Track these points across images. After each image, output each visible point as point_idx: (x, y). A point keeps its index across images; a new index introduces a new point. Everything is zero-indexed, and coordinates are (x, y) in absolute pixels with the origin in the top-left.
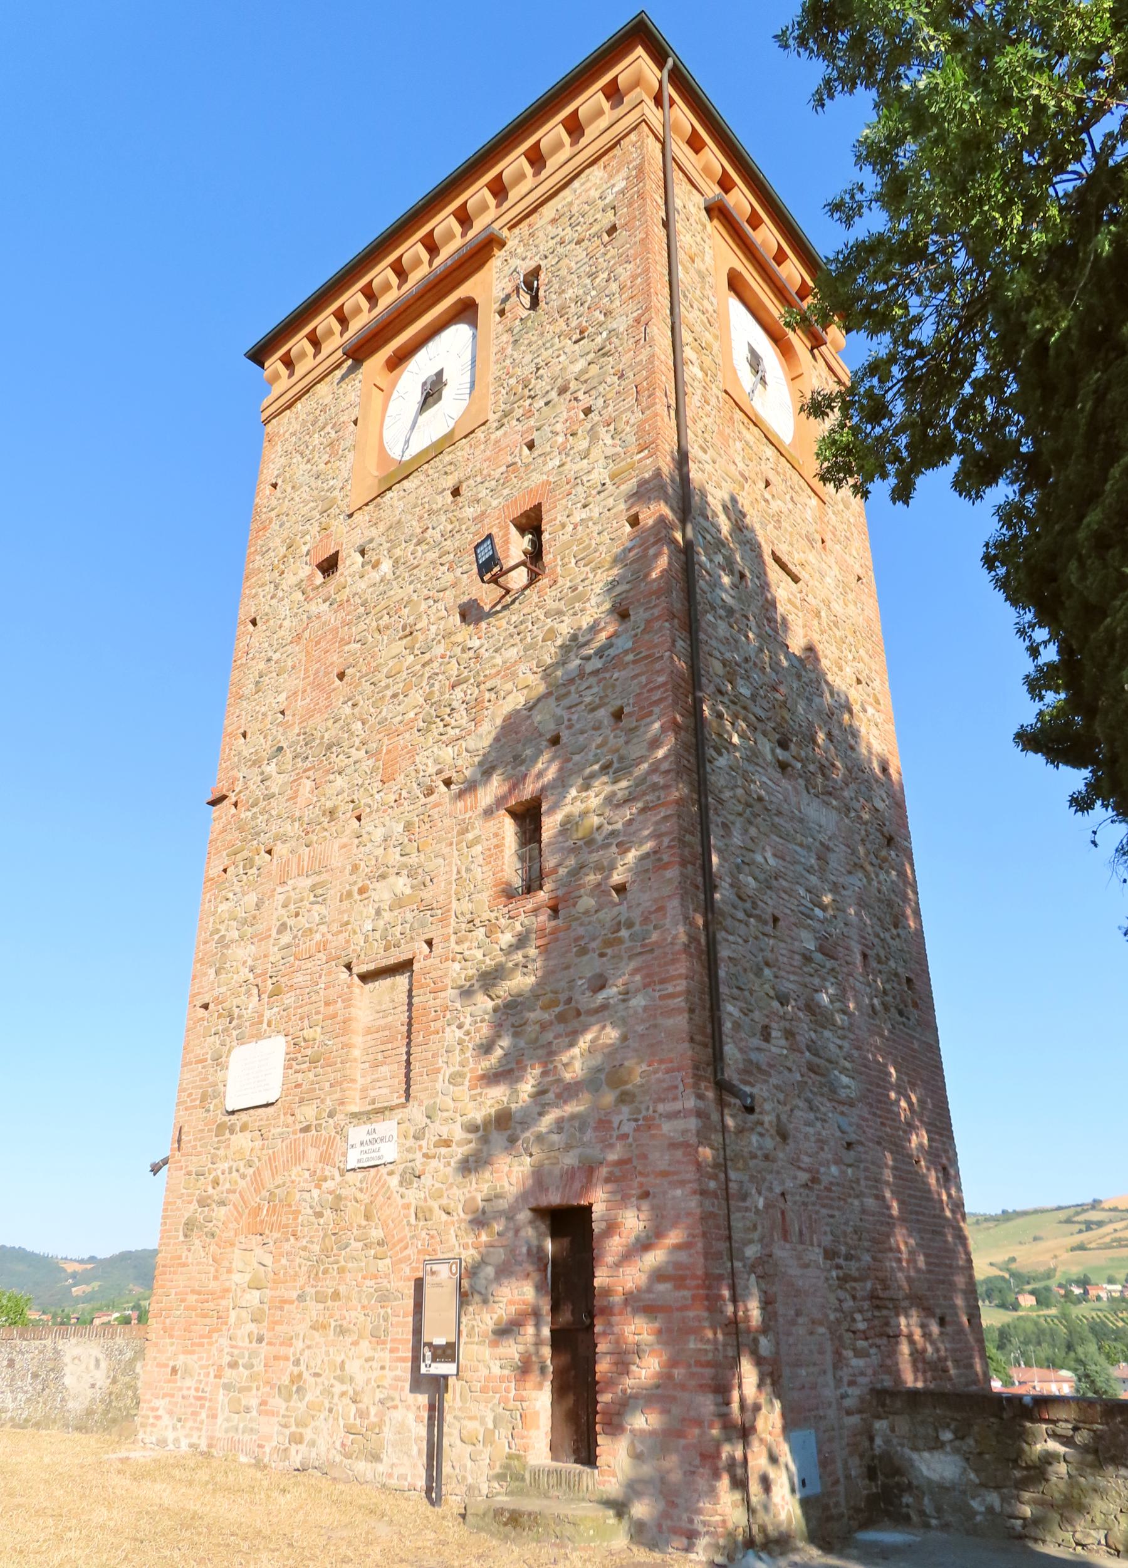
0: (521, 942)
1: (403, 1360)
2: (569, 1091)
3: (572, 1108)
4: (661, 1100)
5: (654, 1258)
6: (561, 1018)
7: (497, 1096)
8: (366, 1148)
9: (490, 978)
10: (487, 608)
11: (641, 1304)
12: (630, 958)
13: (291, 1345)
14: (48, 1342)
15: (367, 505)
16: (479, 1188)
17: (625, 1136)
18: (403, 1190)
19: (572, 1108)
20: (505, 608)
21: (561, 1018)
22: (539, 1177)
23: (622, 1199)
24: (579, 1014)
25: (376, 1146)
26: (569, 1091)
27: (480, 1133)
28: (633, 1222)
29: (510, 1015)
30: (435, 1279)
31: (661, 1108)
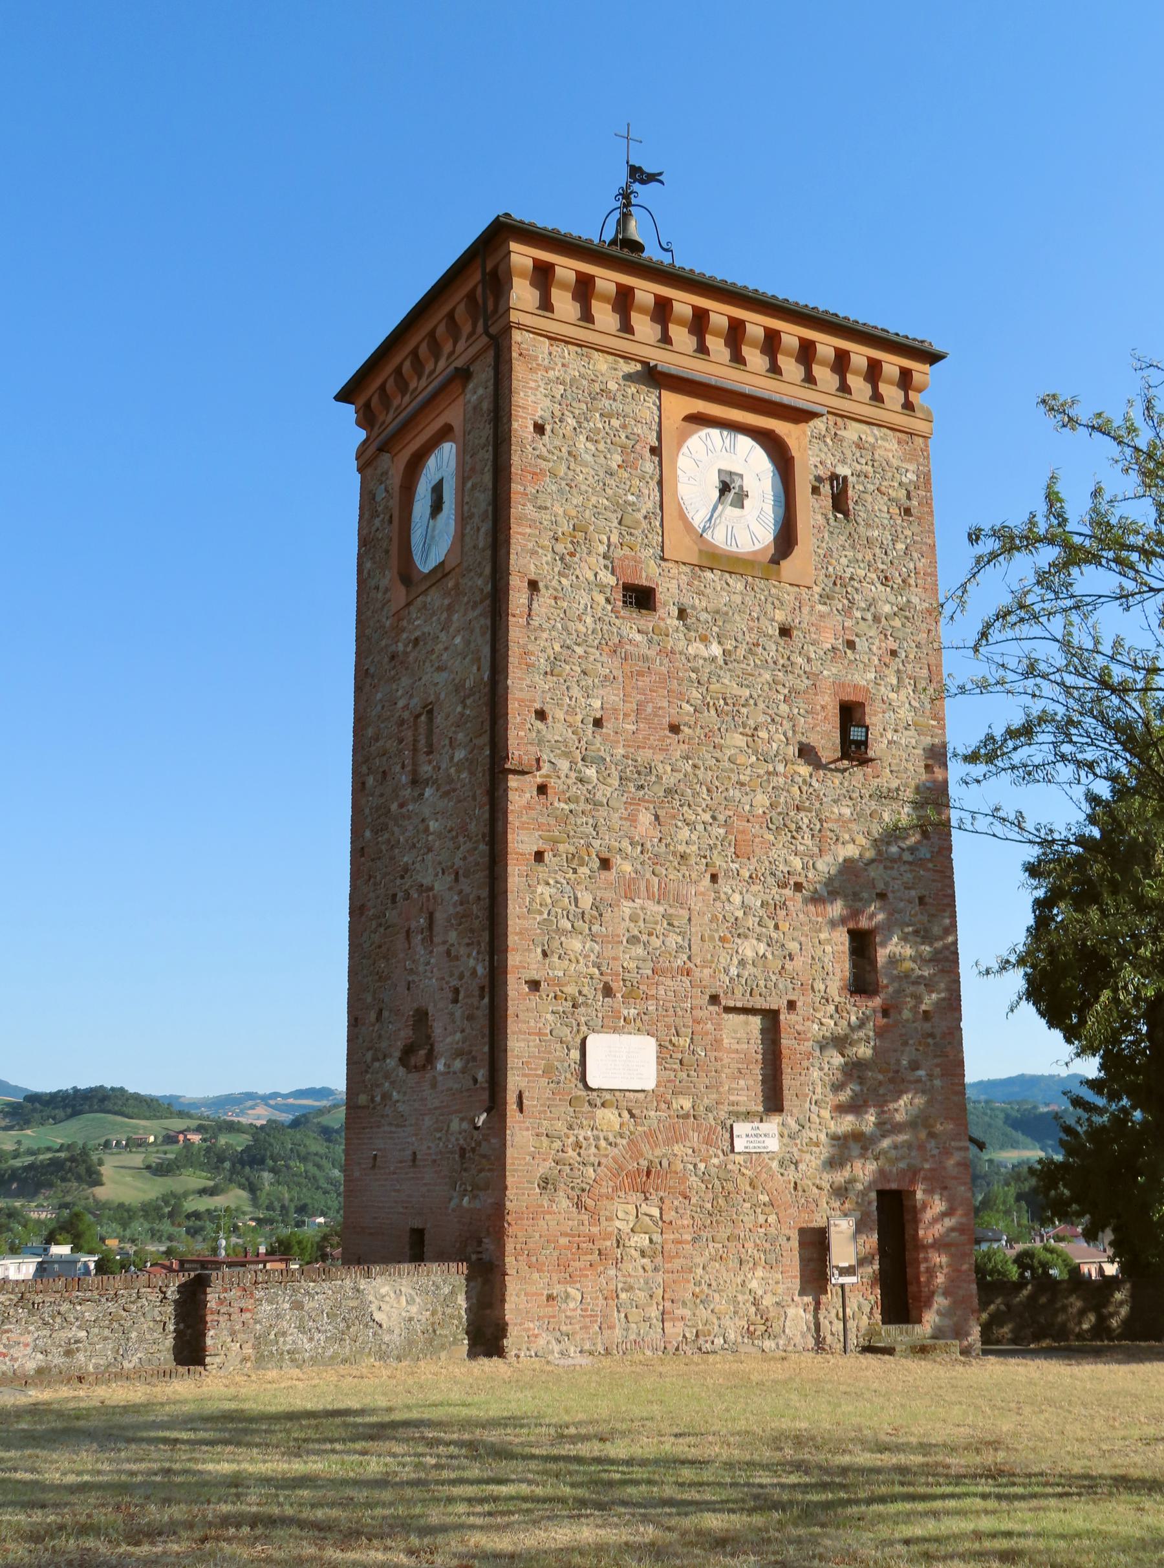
0: (862, 1024)
1: (795, 1277)
2: (898, 1128)
3: (902, 1138)
4: (953, 1140)
5: (948, 1222)
6: (892, 1081)
7: (848, 1123)
8: (751, 1139)
9: (840, 1042)
10: (824, 761)
11: (940, 1245)
12: (935, 1056)
13: (691, 1272)
14: (348, 1283)
15: (684, 564)
16: (840, 1177)
17: (933, 1156)
18: (782, 1171)
19: (902, 1138)
20: (837, 770)
21: (892, 1081)
22: (881, 1172)
23: (929, 1192)
24: (903, 1081)
25: (760, 1139)
26: (898, 1128)
27: (841, 1142)
28: (938, 1205)
29: (854, 1070)
30: (837, 1229)
31: (953, 1144)
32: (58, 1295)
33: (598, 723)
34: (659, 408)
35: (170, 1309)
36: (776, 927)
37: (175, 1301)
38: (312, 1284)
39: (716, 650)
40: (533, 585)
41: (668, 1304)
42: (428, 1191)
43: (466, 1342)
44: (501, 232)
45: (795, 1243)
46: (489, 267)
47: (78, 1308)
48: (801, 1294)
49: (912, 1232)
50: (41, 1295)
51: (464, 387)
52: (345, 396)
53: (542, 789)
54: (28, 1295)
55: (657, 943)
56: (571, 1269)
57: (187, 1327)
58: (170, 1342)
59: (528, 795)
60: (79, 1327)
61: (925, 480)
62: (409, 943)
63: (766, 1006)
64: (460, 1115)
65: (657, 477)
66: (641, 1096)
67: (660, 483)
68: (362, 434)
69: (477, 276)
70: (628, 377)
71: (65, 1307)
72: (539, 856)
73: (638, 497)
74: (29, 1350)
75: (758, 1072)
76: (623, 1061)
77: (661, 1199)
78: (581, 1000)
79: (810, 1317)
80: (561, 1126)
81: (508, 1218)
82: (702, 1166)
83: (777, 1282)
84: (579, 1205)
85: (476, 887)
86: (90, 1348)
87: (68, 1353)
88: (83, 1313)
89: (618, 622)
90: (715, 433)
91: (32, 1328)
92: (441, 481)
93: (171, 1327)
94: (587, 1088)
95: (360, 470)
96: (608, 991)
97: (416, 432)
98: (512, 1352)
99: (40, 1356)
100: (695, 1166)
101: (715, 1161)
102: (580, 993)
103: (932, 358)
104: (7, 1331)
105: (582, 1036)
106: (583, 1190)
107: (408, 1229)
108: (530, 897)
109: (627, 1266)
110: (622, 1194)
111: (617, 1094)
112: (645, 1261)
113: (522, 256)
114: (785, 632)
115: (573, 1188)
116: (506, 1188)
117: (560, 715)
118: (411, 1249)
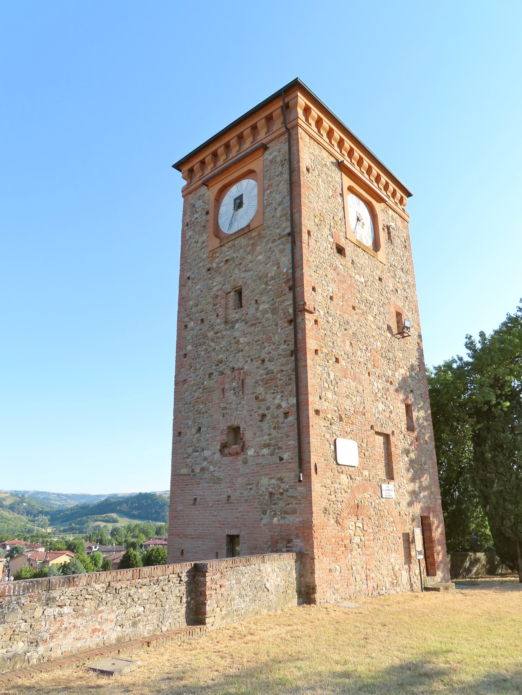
32: (129, 582)
33: (331, 298)
34: (342, 179)
35: (183, 588)
36: (387, 399)
37: (186, 582)
38: (244, 568)
39: (363, 280)
40: (309, 232)
41: (368, 571)
42: (242, 515)
43: (296, 596)
44: (296, 86)
45: (401, 541)
46: (286, 102)
47: (140, 590)
48: (405, 564)
49: (428, 535)
50: (120, 583)
51: (263, 153)
52: (178, 166)
53: (316, 322)
54: (112, 584)
55: (354, 399)
56: (336, 555)
57: (192, 599)
58: (183, 610)
59: (312, 323)
60: (139, 605)
61: (408, 236)
62: (224, 395)
63: (386, 432)
64: (269, 476)
65: (342, 206)
66: (353, 469)
67: (343, 208)
68: (185, 183)
69: (281, 104)
70: (332, 163)
71: (133, 591)
72: (316, 351)
73: (338, 210)
74: (113, 624)
75: (383, 461)
76: (348, 452)
77: (363, 519)
78: (333, 421)
79: (408, 574)
80: (329, 482)
81: (314, 528)
82: (373, 503)
83: (397, 558)
84: (337, 522)
85: (281, 365)
86: (145, 619)
87: (134, 624)
88: (142, 594)
89: (335, 258)
90: (354, 197)
91: (114, 608)
92: (241, 196)
93: (184, 600)
94: (338, 464)
95: (183, 196)
96: (341, 419)
97: (224, 177)
98: (318, 600)
99: (119, 628)
100: (371, 503)
101: (377, 501)
102: (332, 418)
103: (409, 195)
104: (101, 612)
105: (334, 439)
106: (338, 514)
107: (225, 535)
108: (316, 371)
109: (354, 553)
110: (350, 516)
111: (347, 467)
112: (360, 550)
113: (302, 100)
114: (380, 279)
115: (335, 513)
116: (312, 513)
117: (320, 291)
118: (227, 546)
